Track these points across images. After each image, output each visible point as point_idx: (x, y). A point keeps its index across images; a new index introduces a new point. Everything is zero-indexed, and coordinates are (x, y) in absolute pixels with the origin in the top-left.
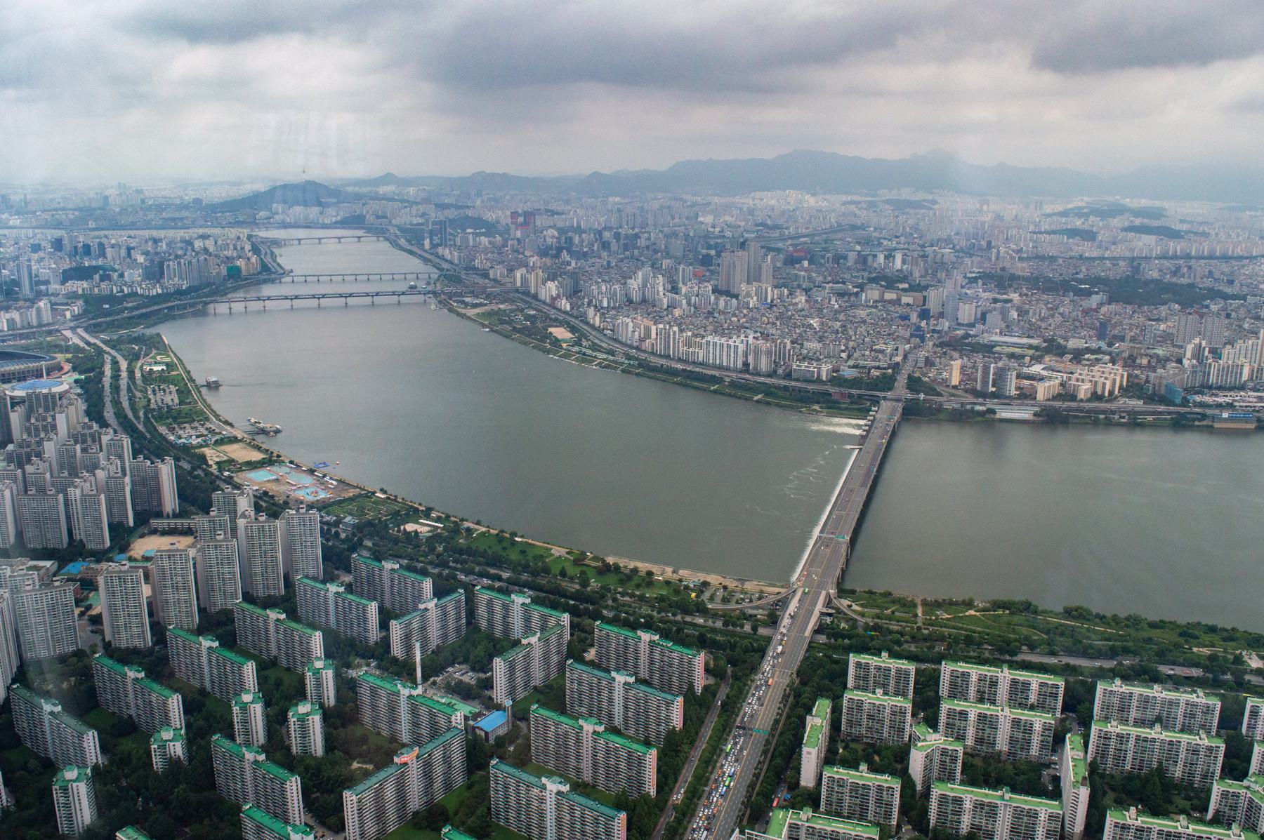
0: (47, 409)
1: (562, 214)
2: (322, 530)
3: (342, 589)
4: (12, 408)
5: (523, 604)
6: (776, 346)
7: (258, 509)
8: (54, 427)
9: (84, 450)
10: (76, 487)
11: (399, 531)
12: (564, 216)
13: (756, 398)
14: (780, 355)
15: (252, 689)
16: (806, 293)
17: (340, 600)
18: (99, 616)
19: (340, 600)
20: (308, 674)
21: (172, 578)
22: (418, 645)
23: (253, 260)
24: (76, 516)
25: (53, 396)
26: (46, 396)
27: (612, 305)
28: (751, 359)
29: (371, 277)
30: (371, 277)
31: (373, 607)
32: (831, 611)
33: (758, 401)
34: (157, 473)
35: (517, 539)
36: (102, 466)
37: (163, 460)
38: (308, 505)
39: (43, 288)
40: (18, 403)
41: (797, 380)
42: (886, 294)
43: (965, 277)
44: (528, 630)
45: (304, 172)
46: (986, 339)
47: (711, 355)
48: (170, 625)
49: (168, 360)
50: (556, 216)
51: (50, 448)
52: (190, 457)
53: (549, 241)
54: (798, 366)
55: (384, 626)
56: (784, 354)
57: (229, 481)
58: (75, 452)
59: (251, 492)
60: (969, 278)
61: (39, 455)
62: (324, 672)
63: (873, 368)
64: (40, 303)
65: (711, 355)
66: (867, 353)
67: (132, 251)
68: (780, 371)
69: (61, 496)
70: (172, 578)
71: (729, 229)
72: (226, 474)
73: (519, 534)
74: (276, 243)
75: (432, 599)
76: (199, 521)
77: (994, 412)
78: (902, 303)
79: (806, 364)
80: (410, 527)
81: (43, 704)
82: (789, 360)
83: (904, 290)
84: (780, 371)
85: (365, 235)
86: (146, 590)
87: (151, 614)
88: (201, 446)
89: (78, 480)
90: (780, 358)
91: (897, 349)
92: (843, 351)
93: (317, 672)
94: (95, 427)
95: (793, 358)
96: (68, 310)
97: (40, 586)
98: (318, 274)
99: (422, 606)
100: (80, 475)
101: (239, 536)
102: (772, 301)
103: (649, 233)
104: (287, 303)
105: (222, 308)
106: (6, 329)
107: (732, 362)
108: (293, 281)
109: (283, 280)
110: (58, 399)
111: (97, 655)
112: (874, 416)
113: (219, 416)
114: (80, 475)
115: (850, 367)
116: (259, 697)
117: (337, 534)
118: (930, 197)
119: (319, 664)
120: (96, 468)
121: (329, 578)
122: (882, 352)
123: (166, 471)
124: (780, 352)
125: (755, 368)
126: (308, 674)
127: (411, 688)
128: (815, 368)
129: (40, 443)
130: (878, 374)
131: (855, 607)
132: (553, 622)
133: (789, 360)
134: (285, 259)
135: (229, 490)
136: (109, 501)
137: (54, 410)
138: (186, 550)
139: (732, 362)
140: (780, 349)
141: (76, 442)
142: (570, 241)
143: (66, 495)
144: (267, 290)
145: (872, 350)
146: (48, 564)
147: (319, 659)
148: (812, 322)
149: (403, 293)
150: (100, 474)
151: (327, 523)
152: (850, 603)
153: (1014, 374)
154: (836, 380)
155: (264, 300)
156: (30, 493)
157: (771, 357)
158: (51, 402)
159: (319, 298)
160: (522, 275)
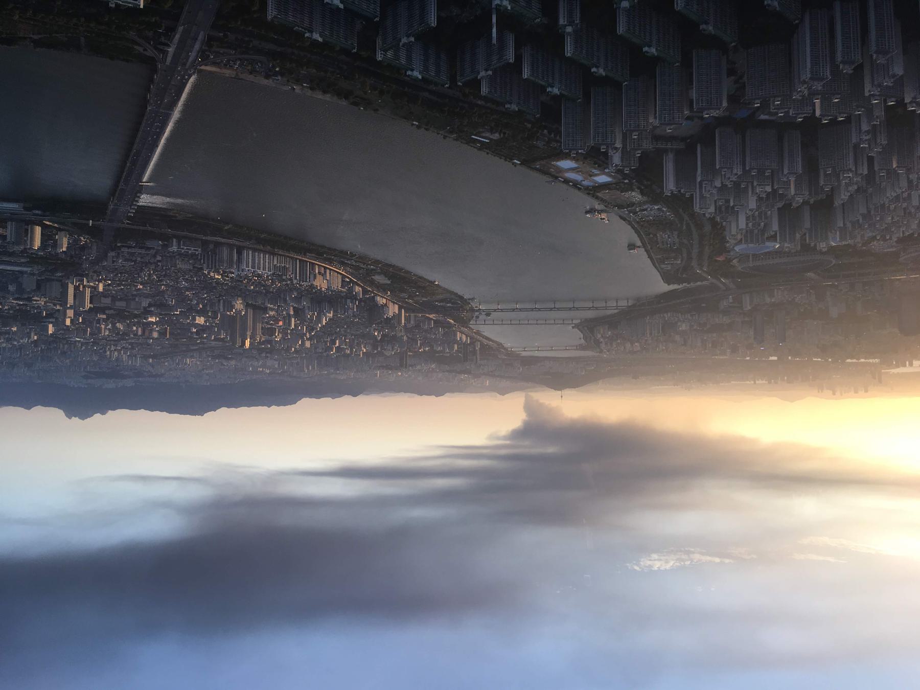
0: (752, 231)
1: (380, 367)
2: (560, 137)
3: (549, 89)
4: (776, 234)
5: (412, 70)
6: (215, 266)
7: (606, 154)
8: (748, 218)
9: (728, 201)
10: (736, 174)
11: (504, 133)
12: (379, 365)
13: (230, 226)
14: (212, 259)
15: (621, 12)
16: (191, 307)
17: (550, 81)
18: (729, 75)
19: (550, 81)
20: (578, 22)
21: (673, 103)
22: (494, 41)
23: (599, 336)
24: (738, 153)
25: (746, 242)
26: (752, 242)
27: (343, 300)
28: (399, 14)
29: (553, 322)
30: (518, 322)
31: (526, 74)
32: (162, 47)
33: (228, 224)
34: (677, 182)
35: (417, 123)
36: (715, 189)
37: (672, 193)
38: (570, 155)
39: (746, 319)
40: (772, 237)
41: (196, 239)
42: (125, 305)
43: (57, 319)
44: (409, 46)
45: (562, 397)
46: (36, 269)
47: (267, 261)
48: (677, 66)
49: (663, 266)
50: (385, 365)
51: (752, 204)
52: (655, 196)
53: (390, 347)
54: (197, 250)
55: (519, 58)
56: (208, 260)
57: (625, 176)
58: (734, 200)
59: (610, 168)
60: (53, 318)
61: (760, 199)
62: (566, 23)
63: (133, 247)
64: (750, 308)
65: (267, 261)
66: (139, 259)
67: (683, 343)
68: (211, 246)
69: (747, 169)
70: (673, 103)
71: (255, 355)
72: (626, 181)
73: (415, 126)
74: (582, 348)
75: (482, 78)
76: (647, 145)
77: (25, 209)
78: (110, 298)
79: (190, 252)
80: (496, 136)
81: (777, 6)
82: (204, 256)
83: (110, 309)
84: (211, 246)
85: (521, 352)
86: (694, 94)
87: (691, 74)
88: (645, 203)
89: (734, 179)
90: (212, 257)
91: (113, 262)
92: (159, 261)
93: (571, 23)
94: (718, 219)
95: (201, 256)
96: (731, 303)
97: (769, 100)
98: (528, 325)
99: (490, 73)
100: (732, 183)
101: (621, 134)
102: (219, 301)
103: (316, 353)
104: (577, 305)
105: (623, 303)
106: (776, 290)
107: (250, 255)
108: (563, 320)
109: (579, 321)
110: (743, 239)
111: (733, 44)
112: (131, 208)
113: (629, 225)
114: (732, 183)
115: (153, 248)
116: (616, 3)
117: (550, 133)
118: (89, 381)
119: (569, 29)
120: (720, 187)
121: (557, 98)
122: (126, 260)
123: (670, 185)
124: (212, 261)
125: (232, 250)
126: (578, 22)
127: (501, 6)
128: (183, 249)
129: (759, 207)
130: (129, 242)
131: (141, 50)
132: (390, 54)
133: (204, 256)
134: (577, 337)
135: (626, 169)
136: (714, 164)
137: (747, 231)
138: (661, 124)
139: (250, 255)
140: (212, 265)
141: (733, 207)
142: (375, 347)
143: (744, 168)
144: (590, 314)
145: (135, 261)
146: (763, 117)
147: (569, 34)
148: (186, 285)
149: (495, 310)
150: (718, 184)
151: (557, 141)
152: (145, 53)
153: (8, 240)
154: (166, 239)
155: (555, 308)
156: (770, 171)
157: (219, 258)
158: (749, 236)
159: (574, 307)
160: (410, 323)
